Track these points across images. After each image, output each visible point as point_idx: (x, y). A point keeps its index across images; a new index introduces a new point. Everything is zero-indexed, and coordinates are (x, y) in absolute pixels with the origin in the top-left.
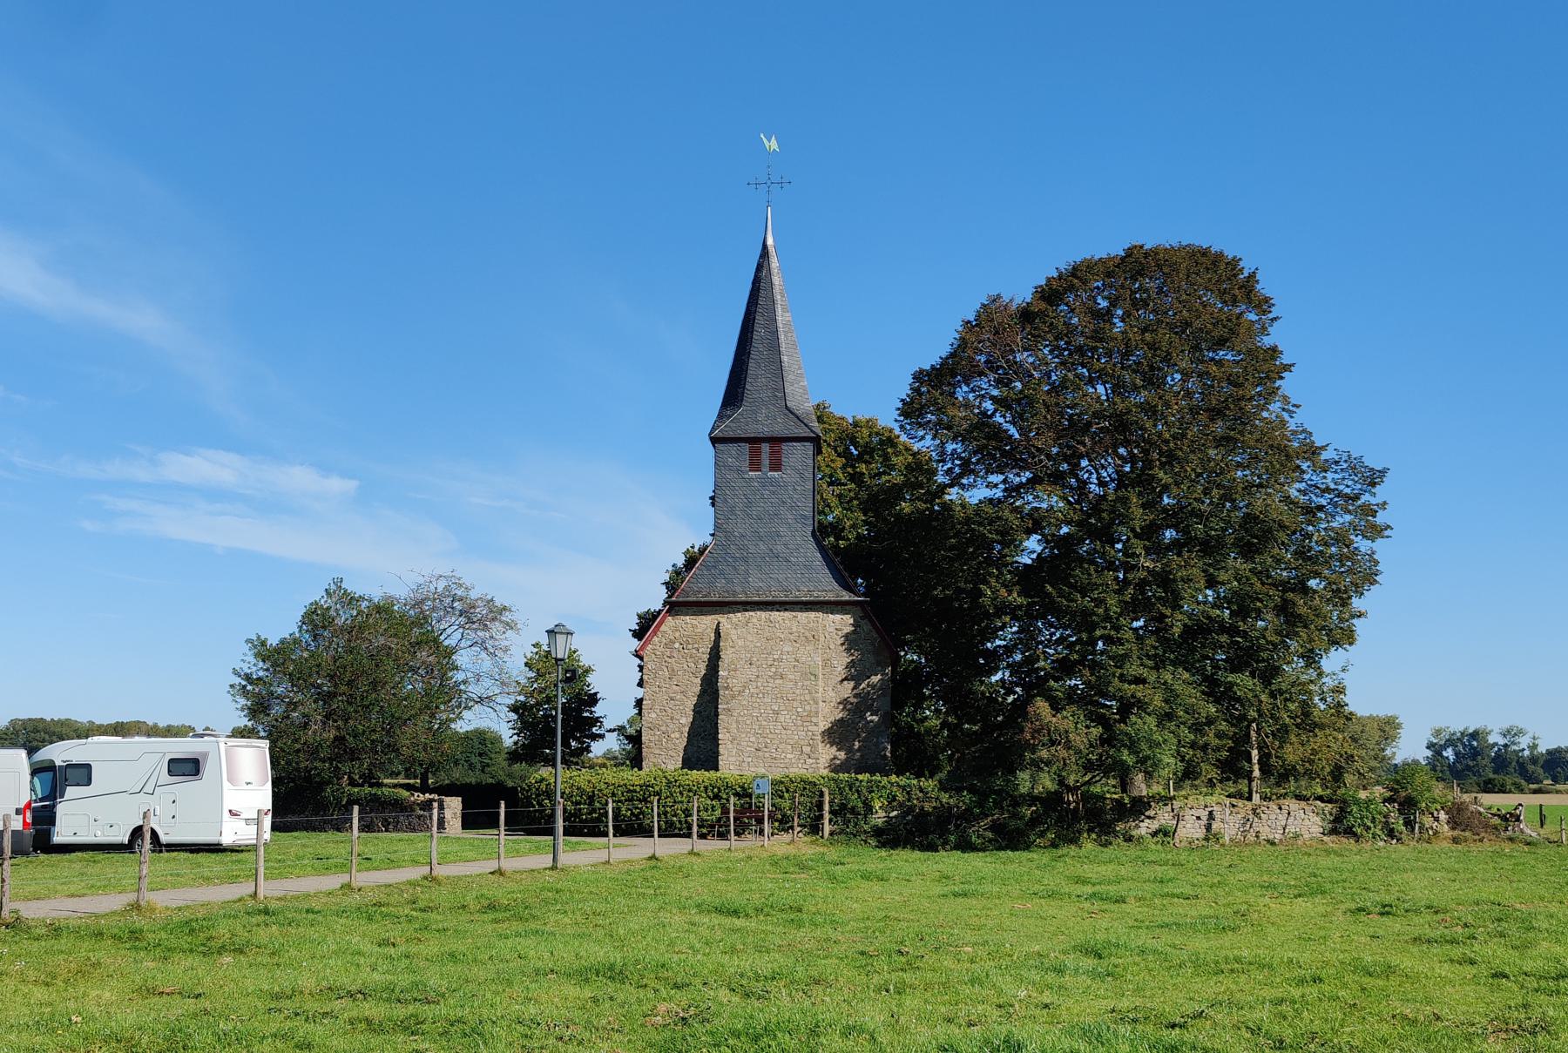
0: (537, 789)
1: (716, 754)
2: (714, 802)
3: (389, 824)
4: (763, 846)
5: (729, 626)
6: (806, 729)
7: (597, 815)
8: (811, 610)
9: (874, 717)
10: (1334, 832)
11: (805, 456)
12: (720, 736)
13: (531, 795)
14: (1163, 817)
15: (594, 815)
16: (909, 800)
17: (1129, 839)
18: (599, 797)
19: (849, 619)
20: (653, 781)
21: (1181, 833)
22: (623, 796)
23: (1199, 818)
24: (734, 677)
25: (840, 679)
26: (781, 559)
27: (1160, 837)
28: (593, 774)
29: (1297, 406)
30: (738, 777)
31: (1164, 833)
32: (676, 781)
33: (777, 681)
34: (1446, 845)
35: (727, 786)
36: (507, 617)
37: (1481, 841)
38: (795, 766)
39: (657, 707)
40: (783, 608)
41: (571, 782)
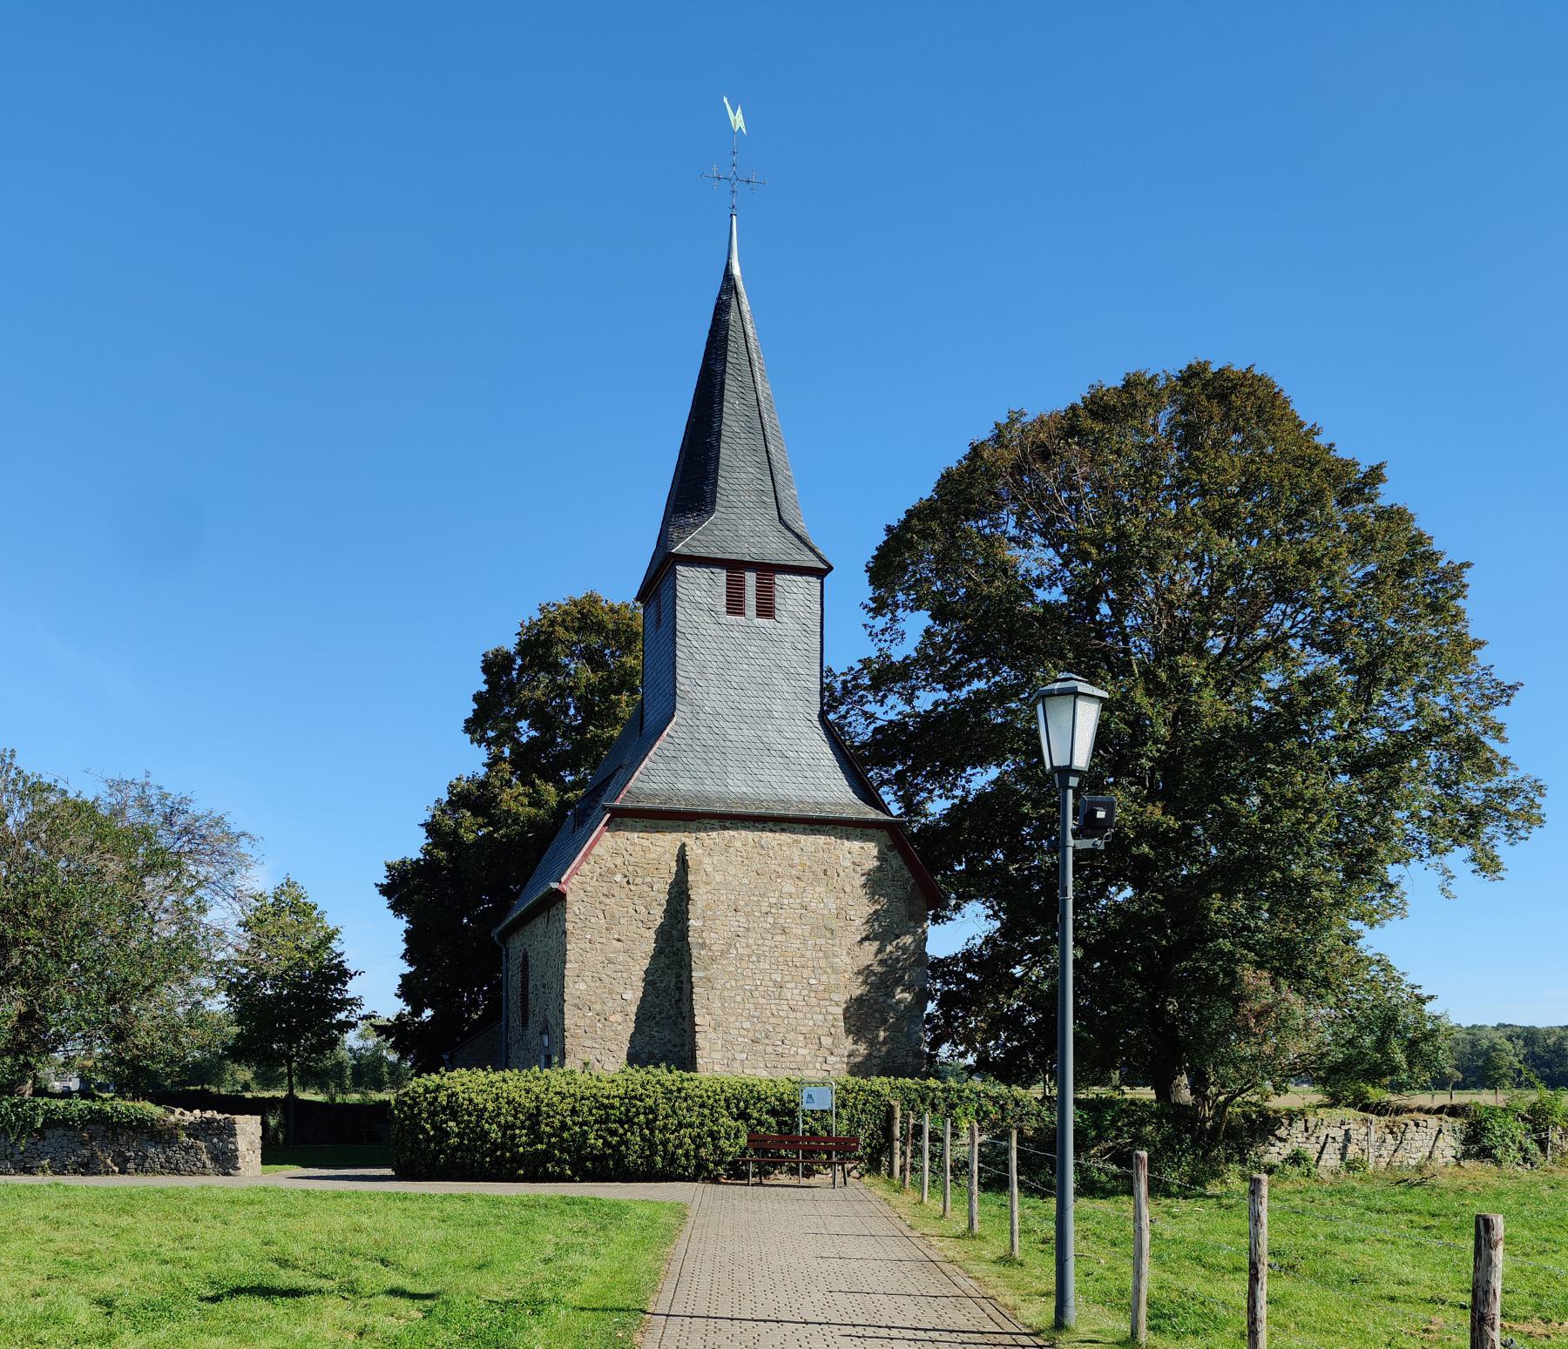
0: (430, 1104)
1: (693, 1048)
2: (738, 1123)
3: (128, 1160)
5: (700, 851)
6: (824, 1011)
8: (820, 832)
9: (906, 995)
11: (808, 597)
12: (697, 1020)
13: (420, 1112)
15: (539, 1146)
16: (1003, 1119)
18: (549, 1116)
19: (872, 849)
20: (641, 1091)
25: (859, 939)
32: (679, 1090)
33: (778, 938)
38: (811, 1066)
39: (588, 973)
40: (778, 828)
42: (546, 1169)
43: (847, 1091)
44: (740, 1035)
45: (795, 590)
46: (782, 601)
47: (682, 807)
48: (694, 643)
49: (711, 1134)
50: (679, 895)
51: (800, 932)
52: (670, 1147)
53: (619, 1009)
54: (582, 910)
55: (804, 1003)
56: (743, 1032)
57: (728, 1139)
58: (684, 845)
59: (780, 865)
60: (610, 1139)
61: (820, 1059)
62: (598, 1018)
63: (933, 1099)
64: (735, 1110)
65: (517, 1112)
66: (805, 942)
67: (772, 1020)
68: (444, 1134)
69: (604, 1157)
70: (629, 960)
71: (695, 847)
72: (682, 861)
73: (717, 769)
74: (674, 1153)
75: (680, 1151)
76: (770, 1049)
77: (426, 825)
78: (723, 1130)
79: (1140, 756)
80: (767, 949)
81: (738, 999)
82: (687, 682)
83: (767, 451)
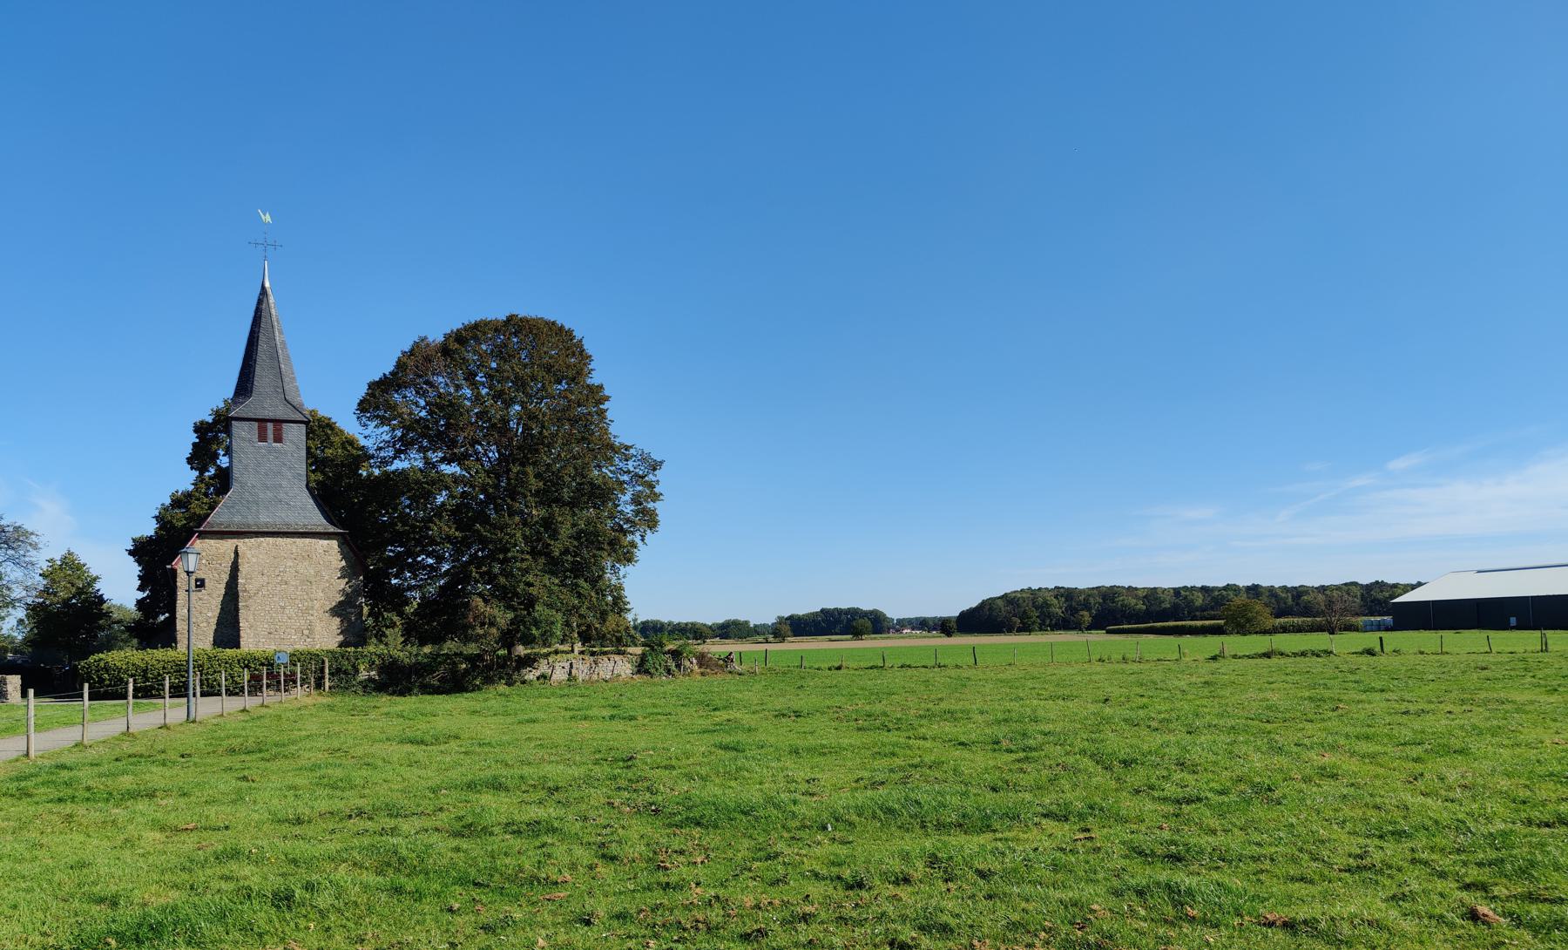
1: (238, 636)
4: (296, 699)
10: (639, 672)
12: (241, 625)
14: (543, 667)
17: (524, 682)
21: (554, 677)
23: (563, 668)
24: (250, 584)
27: (542, 680)
29: (612, 421)
31: (543, 677)
32: (215, 657)
34: (699, 677)
37: (716, 674)
50: (235, 568)
52: (210, 681)
77: (156, 517)
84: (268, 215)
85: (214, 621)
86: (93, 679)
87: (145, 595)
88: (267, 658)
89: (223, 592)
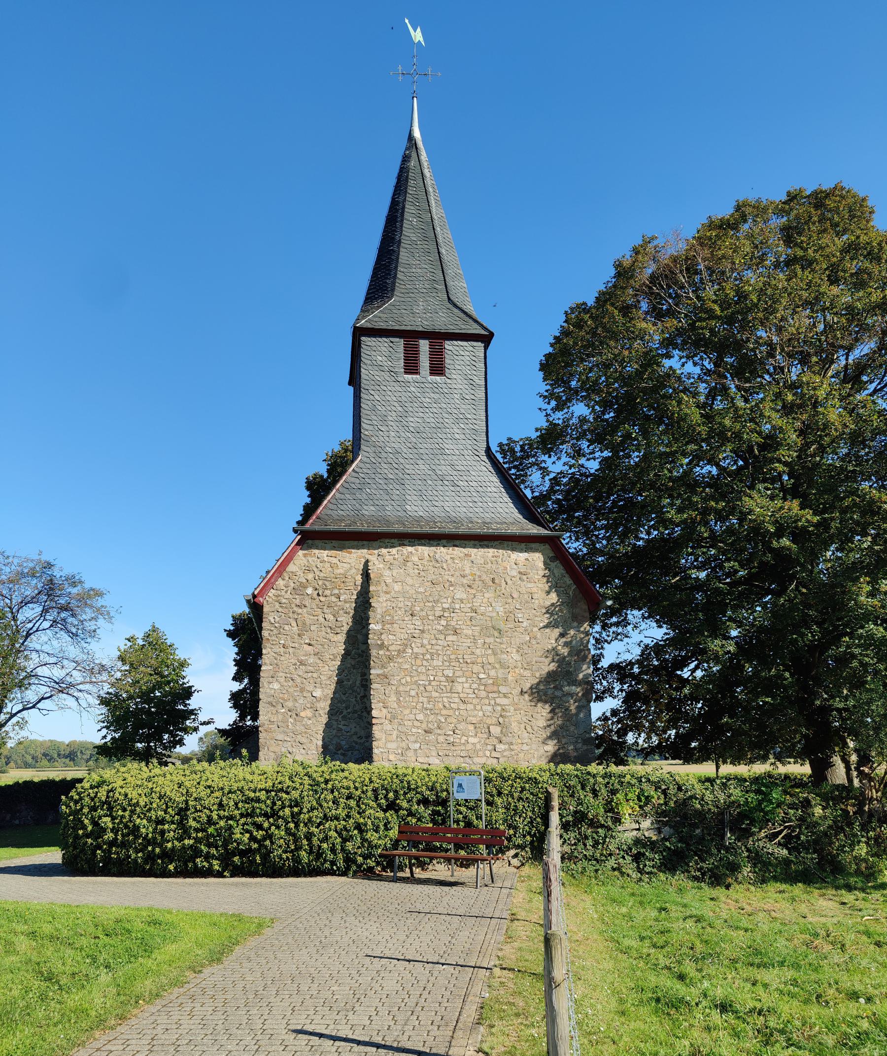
1: (369, 737)
2: (388, 814)
5: (381, 566)
6: (492, 702)
7: (191, 842)
11: (474, 358)
12: (374, 713)
18: (197, 811)
22: (237, 808)
24: (390, 632)
26: (446, 483)
28: (187, 773)
30: (424, 773)
32: (326, 782)
33: (450, 638)
35: (409, 789)
36: (100, 602)
38: (480, 753)
39: (281, 674)
41: (150, 785)
42: (195, 865)
43: (503, 778)
44: (414, 726)
45: (462, 353)
46: (451, 362)
47: (365, 528)
48: (377, 397)
49: (358, 827)
50: (363, 603)
51: (470, 632)
52: (315, 841)
53: (309, 705)
54: (277, 619)
55: (474, 696)
56: (417, 724)
57: (377, 831)
58: (367, 561)
59: (452, 575)
60: (255, 833)
61: (490, 748)
62: (290, 713)
63: (594, 785)
64: (383, 801)
65: (167, 807)
66: (475, 641)
67: (444, 712)
68: (99, 831)
69: (250, 850)
70: (318, 661)
71: (376, 562)
72: (366, 575)
73: (397, 498)
74: (320, 847)
75: (325, 845)
76: (441, 739)
78: (369, 822)
79: (772, 461)
80: (440, 648)
81: (413, 693)
82: (371, 428)
83: (439, 253)
84: (419, 30)
85: (324, 706)
86: (84, 827)
87: (242, 686)
88: (432, 789)
89: (341, 649)
